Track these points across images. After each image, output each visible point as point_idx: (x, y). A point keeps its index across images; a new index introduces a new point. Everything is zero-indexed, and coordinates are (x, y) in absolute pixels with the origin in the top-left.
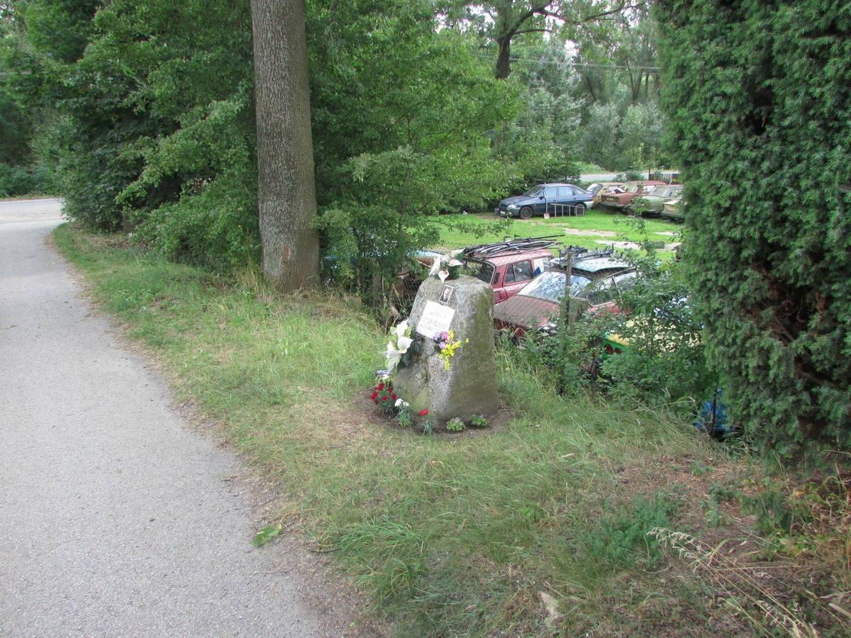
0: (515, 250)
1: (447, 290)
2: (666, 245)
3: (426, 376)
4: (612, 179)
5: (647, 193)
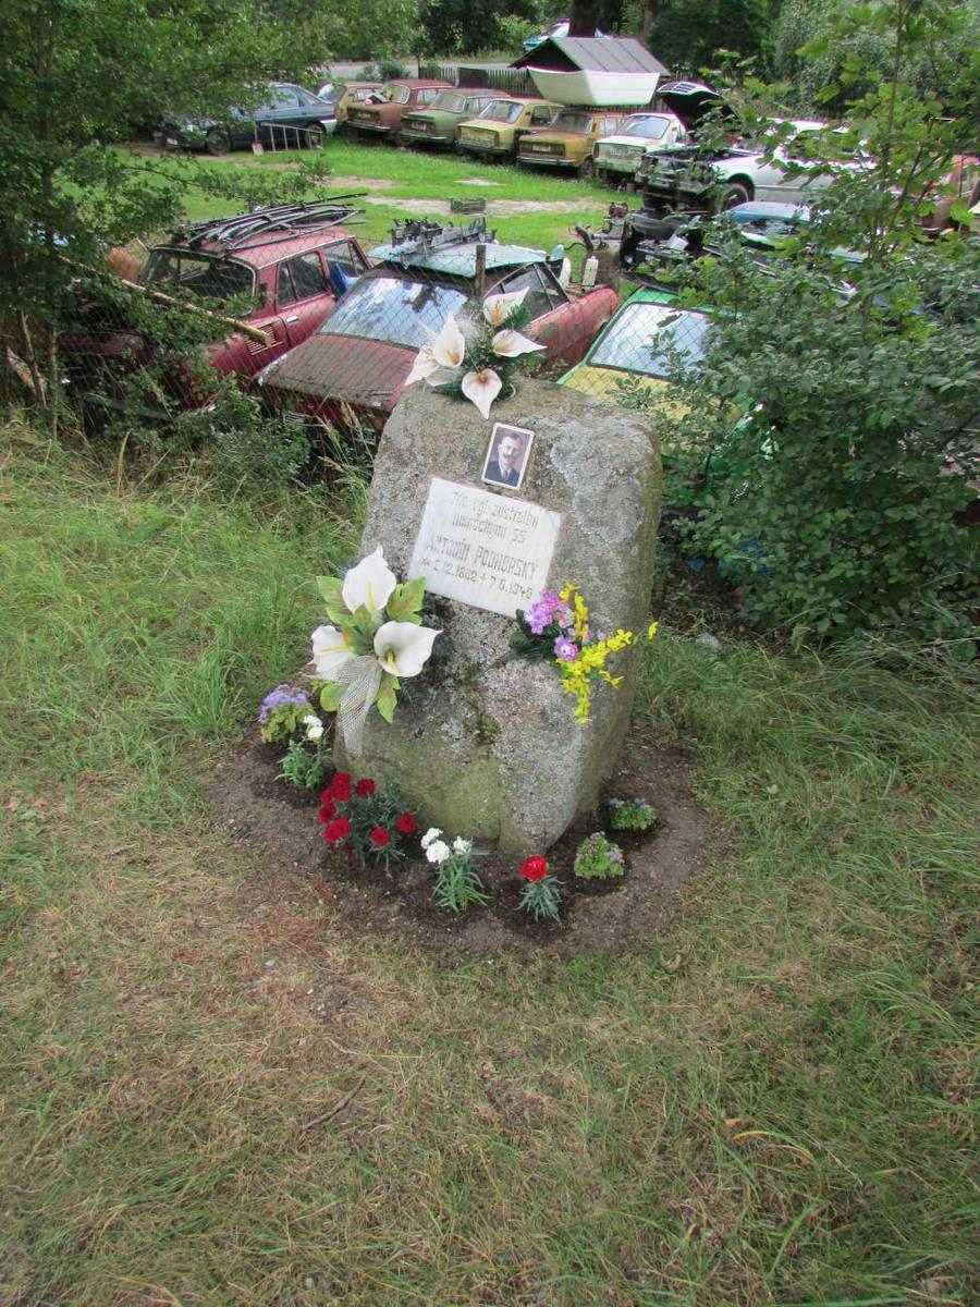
0: (283, 228)
1: (507, 441)
2: (488, 205)
3: (480, 724)
4: (354, 76)
5: (426, 105)
